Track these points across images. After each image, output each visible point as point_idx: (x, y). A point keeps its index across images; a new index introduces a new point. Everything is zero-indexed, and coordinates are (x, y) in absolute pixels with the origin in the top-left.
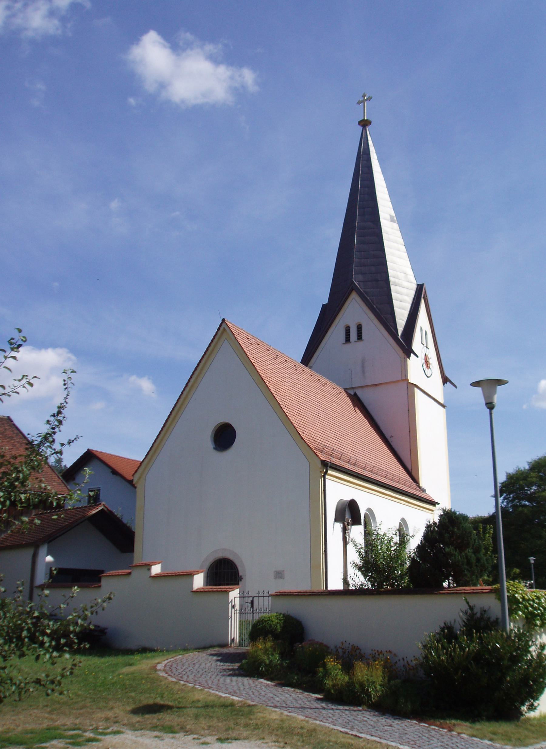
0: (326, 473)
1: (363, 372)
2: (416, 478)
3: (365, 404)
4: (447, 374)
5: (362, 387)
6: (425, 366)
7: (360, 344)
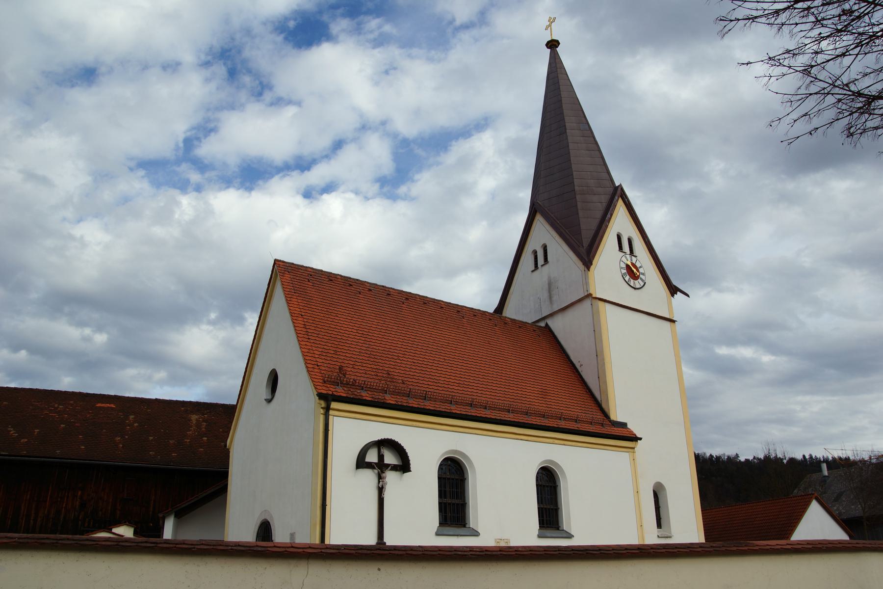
0: (327, 409)
1: (550, 297)
2: (606, 410)
3: (556, 334)
4: (675, 283)
5: (551, 315)
6: (627, 278)
7: (547, 266)
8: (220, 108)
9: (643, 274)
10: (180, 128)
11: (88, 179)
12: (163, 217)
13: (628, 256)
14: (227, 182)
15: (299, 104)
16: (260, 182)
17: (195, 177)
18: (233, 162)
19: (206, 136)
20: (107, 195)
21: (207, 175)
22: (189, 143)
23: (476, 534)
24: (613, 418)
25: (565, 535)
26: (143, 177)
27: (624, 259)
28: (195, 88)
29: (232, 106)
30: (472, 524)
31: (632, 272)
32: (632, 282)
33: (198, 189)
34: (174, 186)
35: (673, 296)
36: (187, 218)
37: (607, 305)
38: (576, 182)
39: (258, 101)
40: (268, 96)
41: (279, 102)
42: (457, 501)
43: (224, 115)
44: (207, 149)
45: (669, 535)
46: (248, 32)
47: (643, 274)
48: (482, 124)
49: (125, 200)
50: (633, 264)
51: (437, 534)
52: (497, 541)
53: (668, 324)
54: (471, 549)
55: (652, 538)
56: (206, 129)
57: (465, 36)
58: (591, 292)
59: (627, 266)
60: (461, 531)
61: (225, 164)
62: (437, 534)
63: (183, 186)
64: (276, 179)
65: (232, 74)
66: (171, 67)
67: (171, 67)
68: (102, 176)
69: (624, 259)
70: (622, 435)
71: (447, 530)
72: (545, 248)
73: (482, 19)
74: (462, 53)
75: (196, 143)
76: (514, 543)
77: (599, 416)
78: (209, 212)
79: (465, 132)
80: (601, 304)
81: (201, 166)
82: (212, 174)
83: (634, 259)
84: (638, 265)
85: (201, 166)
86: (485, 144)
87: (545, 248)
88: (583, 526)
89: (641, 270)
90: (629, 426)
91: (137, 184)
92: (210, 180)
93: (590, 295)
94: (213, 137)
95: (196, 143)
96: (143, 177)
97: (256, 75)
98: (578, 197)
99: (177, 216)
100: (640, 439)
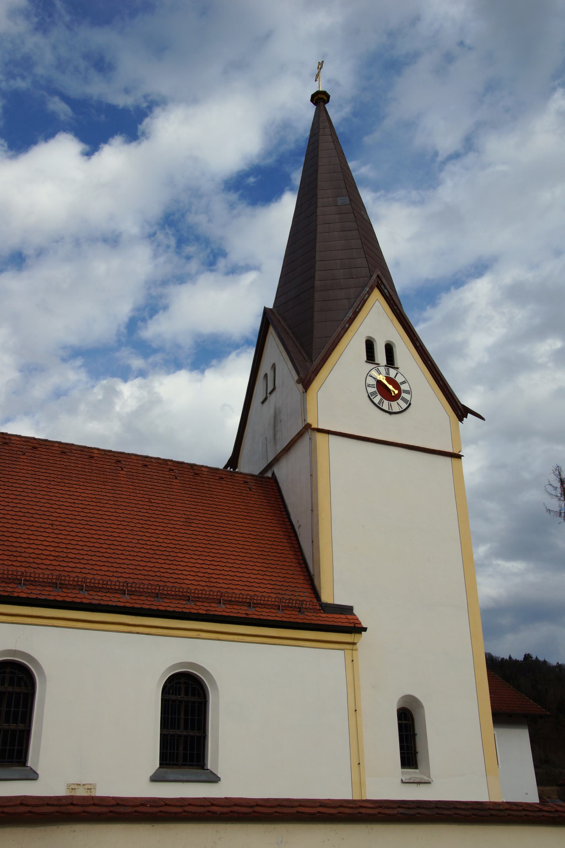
1: (275, 435)
2: (318, 588)
3: (281, 485)
6: (377, 399)
8: (165, 283)
9: (407, 392)
10: (125, 310)
11: (15, 375)
12: (102, 409)
13: (382, 369)
14: (174, 364)
15: (257, 268)
16: (214, 362)
17: (137, 363)
18: (187, 342)
19: (151, 317)
20: (41, 389)
21: (151, 360)
22: (134, 324)
23: (214, 779)
24: (326, 598)
25: (204, 778)
26: (80, 367)
27: (374, 373)
28: (140, 263)
29: (181, 279)
30: (210, 765)
31: (387, 392)
32: (386, 405)
33: (142, 374)
34: (114, 375)
35: (461, 420)
36: (128, 410)
37: (332, 438)
38: (318, 275)
39: (212, 271)
40: (221, 263)
41: (235, 271)
42: (171, 732)
43: (172, 289)
44: (158, 329)
45: (426, 778)
46: (195, 193)
47: (407, 392)
48: (480, 268)
49: (59, 394)
50: (389, 379)
51: (155, 779)
52: (69, 787)
53: (448, 460)
54: (23, 801)
55: (387, 783)
56: (152, 306)
57: (450, 167)
58: (309, 421)
59: (379, 382)
60: (16, 770)
61: (178, 347)
62: (155, 779)
63: (125, 374)
64: (233, 355)
65: (181, 242)
66: (112, 240)
67: (112, 240)
68: (31, 370)
69: (374, 373)
70: (342, 624)
71: (171, 772)
72: (389, 349)
73: (469, 144)
74: (452, 189)
75: (140, 324)
76: (102, 791)
77: (306, 596)
78: (156, 401)
79: (457, 281)
80: (319, 436)
81: (145, 349)
82: (158, 358)
83: (392, 373)
84: (399, 379)
85: (145, 349)
86: (481, 290)
87: (389, 349)
88: (242, 761)
89: (404, 387)
90: (355, 611)
91: (72, 375)
92: (154, 365)
93: (308, 427)
94: (161, 317)
95: (140, 324)
96: (80, 367)
97: (202, 240)
98: (317, 296)
99: (118, 408)
100: (365, 629)
